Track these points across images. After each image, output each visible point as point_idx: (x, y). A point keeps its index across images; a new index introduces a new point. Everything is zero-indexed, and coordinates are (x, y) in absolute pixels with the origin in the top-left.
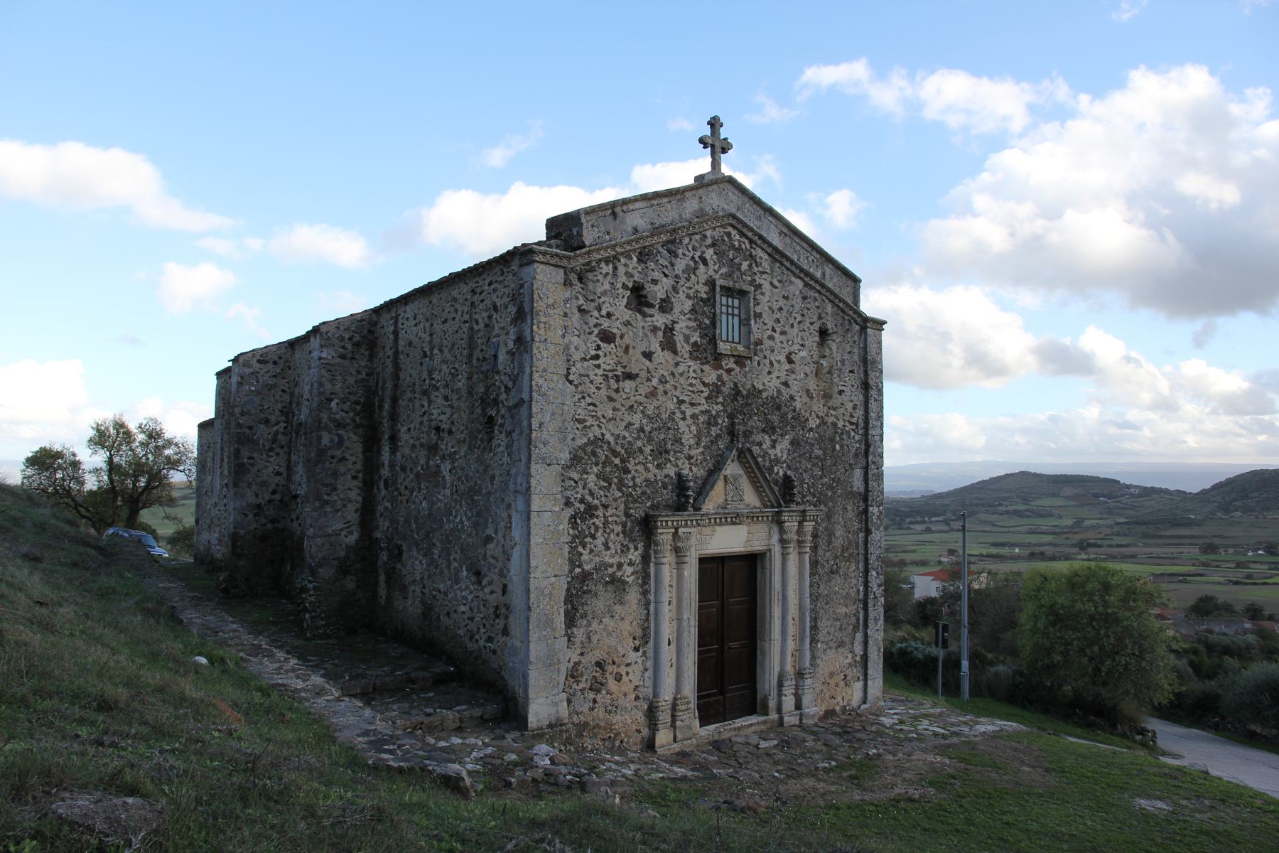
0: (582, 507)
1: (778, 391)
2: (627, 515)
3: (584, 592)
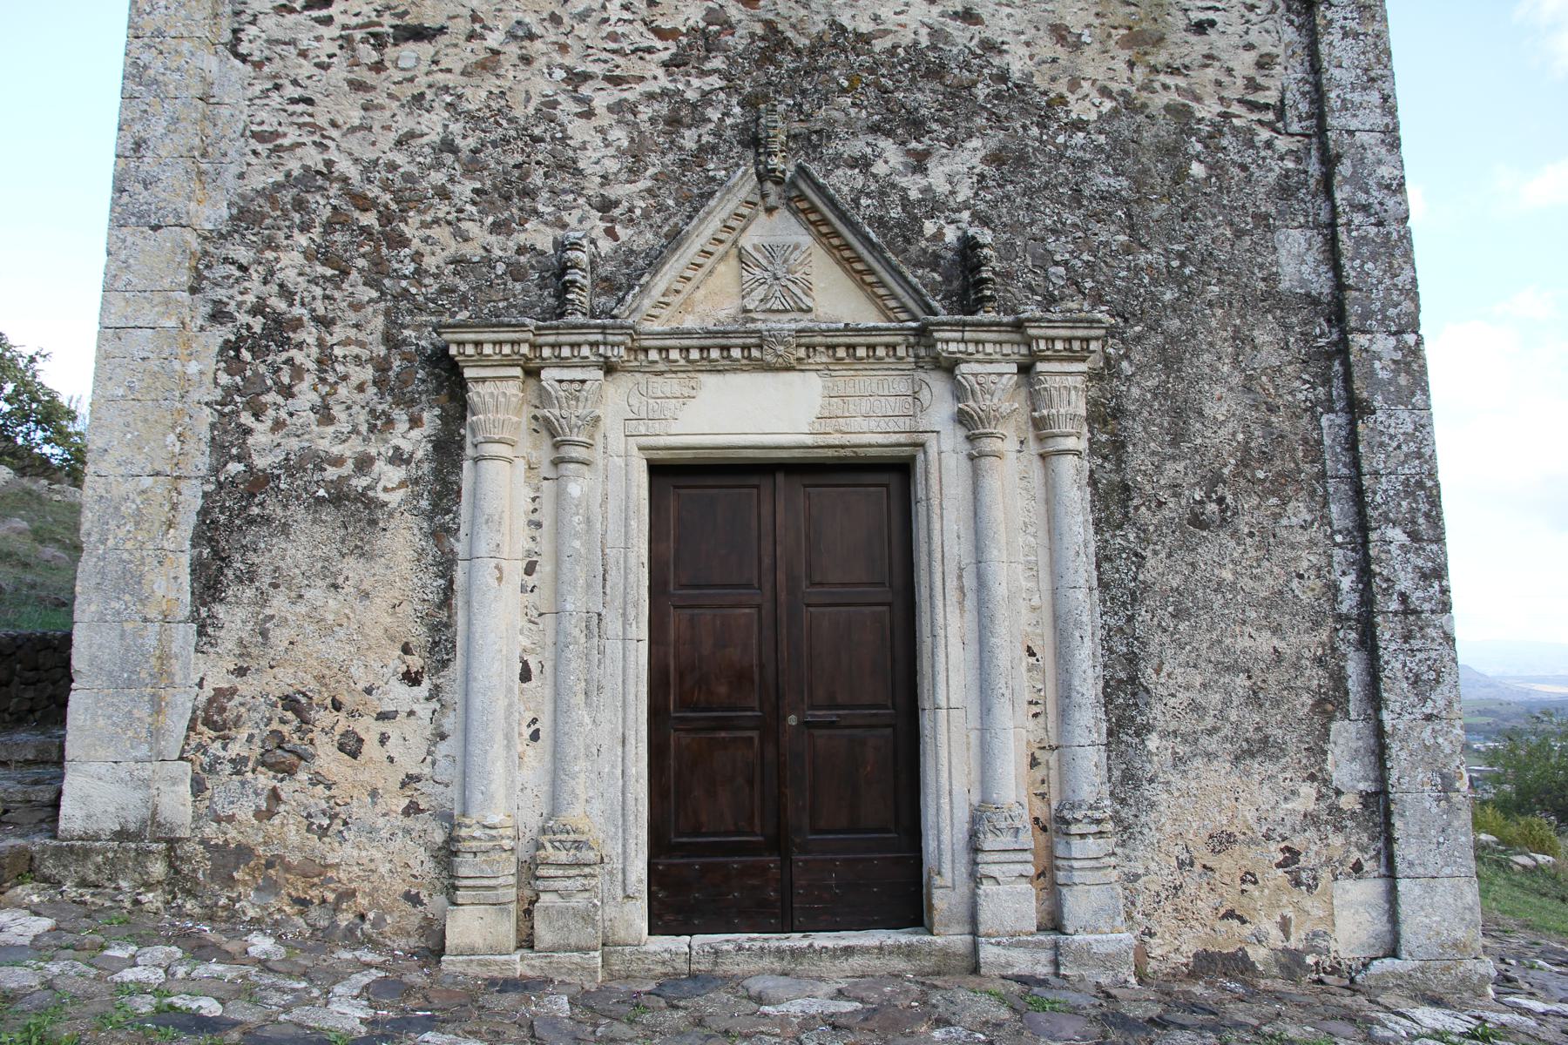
0: (257, 324)
1: (934, 33)
2: (390, 340)
3: (251, 521)
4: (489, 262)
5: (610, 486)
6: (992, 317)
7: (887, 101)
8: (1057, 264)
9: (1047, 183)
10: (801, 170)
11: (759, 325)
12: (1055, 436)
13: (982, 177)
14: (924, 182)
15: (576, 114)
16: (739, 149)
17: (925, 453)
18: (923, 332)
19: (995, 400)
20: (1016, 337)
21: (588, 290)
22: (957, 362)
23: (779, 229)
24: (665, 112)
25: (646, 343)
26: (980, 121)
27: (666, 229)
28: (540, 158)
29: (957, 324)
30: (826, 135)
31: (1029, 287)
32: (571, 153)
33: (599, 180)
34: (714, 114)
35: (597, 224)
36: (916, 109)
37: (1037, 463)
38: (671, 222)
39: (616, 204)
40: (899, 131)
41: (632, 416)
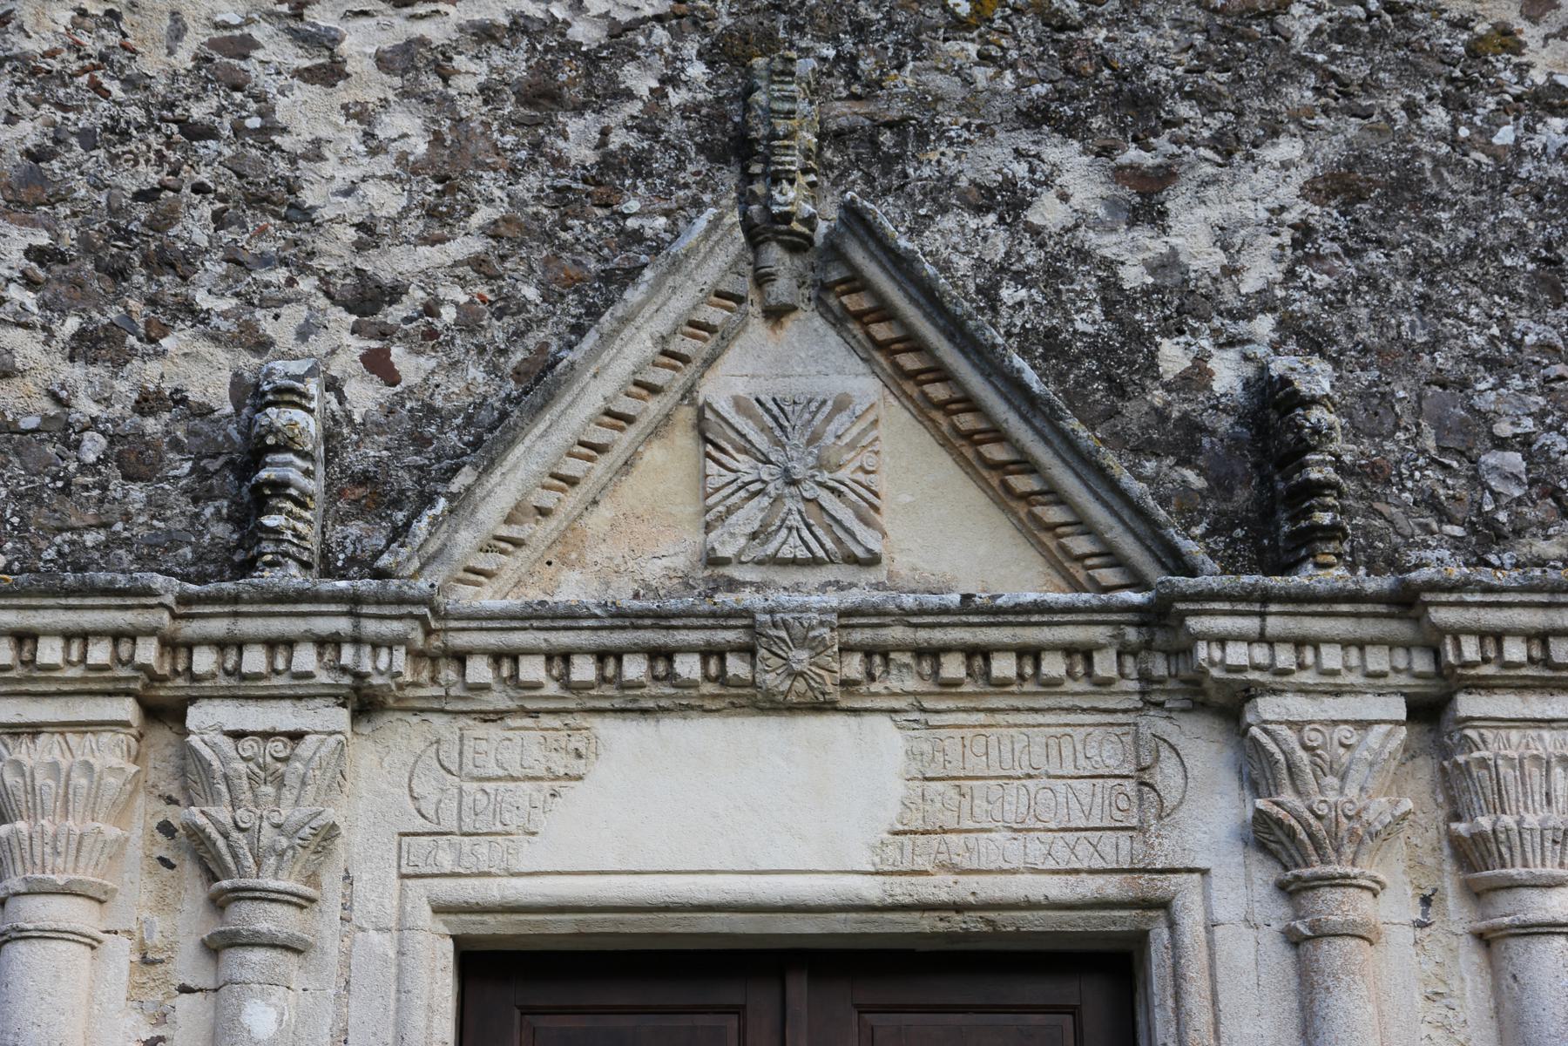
4: (65, 432)
5: (356, 1011)
6: (1337, 576)
7: (1067, 50)
8: (1501, 444)
9: (1471, 246)
10: (854, 217)
11: (748, 598)
12: (1513, 885)
13: (1304, 231)
14: (1159, 247)
15: (299, 74)
16: (700, 164)
17: (1172, 925)
18: (1161, 621)
19: (1352, 791)
20: (1398, 629)
21: (317, 505)
22: (1249, 692)
23: (794, 361)
24: (519, 72)
25: (460, 640)
26: (1299, 95)
27: (518, 356)
28: (204, 176)
29: (1246, 596)
30: (916, 131)
31: (1432, 503)
32: (282, 167)
33: (351, 234)
34: (640, 80)
35: (344, 342)
36: (1138, 69)
37: (1470, 959)
38: (531, 342)
39: (395, 293)
40: (1097, 122)
41: (419, 824)
